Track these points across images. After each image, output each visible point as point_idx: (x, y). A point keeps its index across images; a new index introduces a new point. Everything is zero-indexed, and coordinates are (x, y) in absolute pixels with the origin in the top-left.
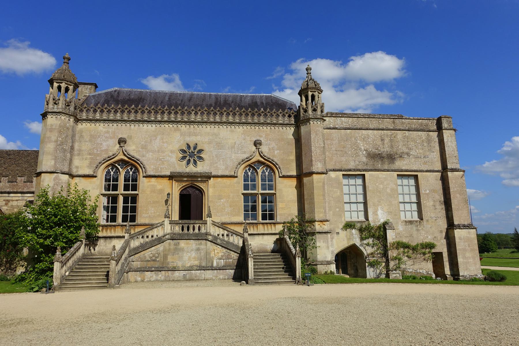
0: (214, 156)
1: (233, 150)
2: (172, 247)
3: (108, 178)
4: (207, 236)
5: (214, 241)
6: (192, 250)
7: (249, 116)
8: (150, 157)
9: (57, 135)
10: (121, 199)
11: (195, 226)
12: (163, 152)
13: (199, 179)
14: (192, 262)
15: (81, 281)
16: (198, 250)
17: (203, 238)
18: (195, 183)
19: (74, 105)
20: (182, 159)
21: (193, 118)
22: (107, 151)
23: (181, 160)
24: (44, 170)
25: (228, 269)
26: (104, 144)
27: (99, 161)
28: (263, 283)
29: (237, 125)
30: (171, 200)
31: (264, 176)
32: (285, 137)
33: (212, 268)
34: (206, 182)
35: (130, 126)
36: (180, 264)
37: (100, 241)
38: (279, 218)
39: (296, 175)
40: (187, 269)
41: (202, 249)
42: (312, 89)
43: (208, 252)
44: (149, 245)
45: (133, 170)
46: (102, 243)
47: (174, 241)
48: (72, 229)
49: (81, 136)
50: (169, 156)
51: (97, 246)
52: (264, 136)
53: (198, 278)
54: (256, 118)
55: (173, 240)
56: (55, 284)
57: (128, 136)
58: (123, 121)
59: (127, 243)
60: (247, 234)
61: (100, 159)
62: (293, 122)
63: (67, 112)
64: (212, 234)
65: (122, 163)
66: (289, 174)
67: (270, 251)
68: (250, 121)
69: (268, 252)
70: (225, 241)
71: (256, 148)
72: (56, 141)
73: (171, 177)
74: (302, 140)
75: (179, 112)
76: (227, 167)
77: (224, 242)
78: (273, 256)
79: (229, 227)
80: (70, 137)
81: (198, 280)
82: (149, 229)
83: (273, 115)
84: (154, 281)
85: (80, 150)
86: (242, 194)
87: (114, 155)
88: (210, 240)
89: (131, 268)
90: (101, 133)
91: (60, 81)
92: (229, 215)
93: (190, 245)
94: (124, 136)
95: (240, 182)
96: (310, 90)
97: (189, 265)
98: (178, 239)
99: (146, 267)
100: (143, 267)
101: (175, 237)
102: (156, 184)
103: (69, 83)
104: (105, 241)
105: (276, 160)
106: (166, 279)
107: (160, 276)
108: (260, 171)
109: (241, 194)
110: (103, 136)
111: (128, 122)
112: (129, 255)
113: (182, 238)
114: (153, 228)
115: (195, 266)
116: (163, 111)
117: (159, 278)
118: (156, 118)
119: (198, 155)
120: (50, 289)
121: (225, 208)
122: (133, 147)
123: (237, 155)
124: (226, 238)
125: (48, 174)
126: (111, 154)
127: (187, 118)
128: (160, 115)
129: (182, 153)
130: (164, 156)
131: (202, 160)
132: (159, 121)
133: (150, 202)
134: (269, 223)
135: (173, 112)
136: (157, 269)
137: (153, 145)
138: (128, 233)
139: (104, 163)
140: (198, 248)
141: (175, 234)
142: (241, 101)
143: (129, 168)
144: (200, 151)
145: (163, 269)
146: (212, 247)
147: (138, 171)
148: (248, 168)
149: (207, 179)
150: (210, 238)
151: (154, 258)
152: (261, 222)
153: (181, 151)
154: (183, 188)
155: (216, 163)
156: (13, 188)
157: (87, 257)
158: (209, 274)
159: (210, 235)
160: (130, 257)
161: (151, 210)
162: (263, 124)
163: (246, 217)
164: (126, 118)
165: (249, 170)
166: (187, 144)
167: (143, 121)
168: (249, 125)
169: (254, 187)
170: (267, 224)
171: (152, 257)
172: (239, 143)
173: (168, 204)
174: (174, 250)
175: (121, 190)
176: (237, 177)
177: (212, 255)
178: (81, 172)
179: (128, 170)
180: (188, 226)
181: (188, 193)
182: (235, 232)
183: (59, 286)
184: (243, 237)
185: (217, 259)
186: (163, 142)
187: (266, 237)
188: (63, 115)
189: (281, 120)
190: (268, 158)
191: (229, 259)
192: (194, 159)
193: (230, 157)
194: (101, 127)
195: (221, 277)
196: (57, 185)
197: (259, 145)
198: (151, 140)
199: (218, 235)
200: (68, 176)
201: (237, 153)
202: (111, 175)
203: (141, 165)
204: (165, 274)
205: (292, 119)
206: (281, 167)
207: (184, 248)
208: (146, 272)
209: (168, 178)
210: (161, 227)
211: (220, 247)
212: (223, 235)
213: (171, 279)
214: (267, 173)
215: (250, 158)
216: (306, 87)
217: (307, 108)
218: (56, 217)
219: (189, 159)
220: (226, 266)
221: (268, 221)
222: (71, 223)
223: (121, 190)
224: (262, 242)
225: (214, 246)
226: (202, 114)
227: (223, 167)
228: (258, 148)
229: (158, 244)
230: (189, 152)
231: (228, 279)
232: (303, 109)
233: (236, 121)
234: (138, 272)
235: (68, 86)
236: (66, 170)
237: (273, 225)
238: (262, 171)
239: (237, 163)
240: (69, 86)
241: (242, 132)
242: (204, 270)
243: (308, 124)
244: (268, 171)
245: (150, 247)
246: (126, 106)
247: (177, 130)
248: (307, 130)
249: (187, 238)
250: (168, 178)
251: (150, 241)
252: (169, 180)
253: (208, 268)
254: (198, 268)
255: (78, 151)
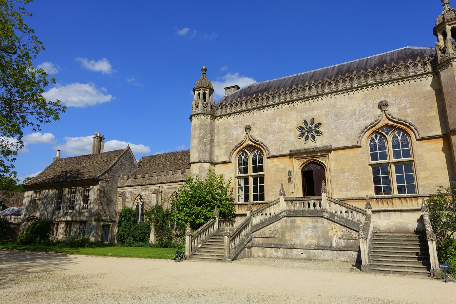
0: (333, 128)
1: (354, 118)
2: (289, 224)
3: (240, 162)
4: (323, 214)
5: (332, 218)
6: (309, 228)
7: (369, 77)
8: (272, 138)
9: (199, 132)
10: (251, 180)
11: (310, 203)
12: (282, 132)
13: (319, 154)
14: (310, 241)
15: (207, 253)
16: (315, 227)
17: (319, 215)
18: (316, 159)
19: (210, 105)
20: (300, 136)
21: (308, 94)
22: (237, 139)
23: (300, 137)
24: (192, 162)
25: (350, 251)
26: (235, 133)
27: (232, 149)
28: (381, 271)
29: (356, 89)
30: (293, 178)
31: (396, 142)
32: (420, 90)
33: (331, 249)
34: (326, 156)
35: (253, 114)
36: (297, 242)
37: (238, 218)
38: (421, 191)
39: (441, 134)
40: (304, 248)
41: (319, 227)
42: (451, 21)
43: (325, 230)
44: (267, 223)
45: (259, 153)
46: (239, 220)
47: (290, 218)
48: (209, 208)
49: (219, 130)
50: (288, 135)
51: (235, 223)
52: (390, 95)
53: (316, 258)
54: (378, 77)
55: (289, 217)
56: (187, 254)
57: (252, 123)
58: (247, 110)
59: (249, 221)
60: (370, 211)
61: (232, 147)
62: (430, 70)
63: (205, 112)
64: (329, 210)
65: (250, 148)
66: (430, 134)
67: (413, 231)
68: (371, 82)
69: (410, 233)
70: (344, 219)
71: (382, 111)
72: (199, 137)
73: (291, 155)
74: (444, 88)
75: (294, 91)
76: (349, 138)
77: (343, 220)
78: (407, 238)
79: (347, 203)
80: (209, 132)
81: (317, 260)
82: (267, 206)
83: (400, 69)
84: (274, 258)
85: (218, 142)
86: (370, 165)
87: (243, 142)
88: (326, 217)
89: (254, 244)
90: (232, 125)
91: (206, 89)
92: (355, 190)
93: (306, 223)
94: (249, 124)
95: (366, 151)
96: (447, 24)
97: (306, 244)
98: (293, 217)
99: (266, 244)
100: (264, 244)
101: (291, 214)
102: (278, 163)
103: (205, 89)
104: (241, 218)
105: (409, 120)
106: (285, 257)
107: (279, 253)
108: (390, 138)
109: (368, 166)
110: (234, 127)
111: (251, 111)
112: (252, 231)
113: (298, 216)
114: (270, 206)
115: (313, 245)
116: (279, 94)
117: (279, 255)
118: (274, 101)
119: (316, 129)
120: (182, 258)
121: (350, 182)
122: (257, 132)
123: (359, 123)
124: (345, 215)
125: (195, 164)
126: (240, 141)
127: (302, 95)
128: (277, 98)
129: (300, 130)
130: (283, 136)
131: (320, 134)
132: (276, 104)
133: (275, 181)
134: (413, 197)
135: (288, 92)
136: (276, 246)
137: (274, 127)
138: (249, 211)
139: (235, 150)
140: (315, 225)
141: (290, 211)
142: (367, 64)
143: (255, 152)
144: (318, 125)
145: (281, 247)
146: (330, 225)
147: (263, 154)
148: (374, 135)
149: (327, 153)
150: (326, 215)
151: (273, 235)
152: (397, 196)
153: (299, 128)
154: (304, 165)
155: (336, 135)
156: (184, 178)
157: (220, 232)
158: (328, 255)
159: (327, 212)
160: (252, 233)
161: (276, 188)
162: (387, 81)
163: (378, 191)
164: (249, 108)
165: (376, 137)
166: (304, 121)
167: (263, 107)
168: (370, 87)
169: (384, 156)
170: (405, 198)
171: (271, 234)
172: (360, 109)
173: (291, 182)
174: (291, 228)
175: (251, 172)
176: (360, 147)
177: (330, 233)
178: (220, 160)
179: (255, 153)
180: (309, 202)
181: (309, 170)
182: (354, 209)
183: (190, 256)
184: (365, 214)
185: (336, 238)
186: (282, 123)
187: (405, 214)
188: (202, 115)
189: (412, 72)
190: (398, 120)
191: (350, 239)
192: (312, 135)
193: (351, 126)
194: (231, 120)
195: (343, 259)
196: (202, 172)
197: (384, 107)
198: (271, 123)
199: (336, 212)
200: (209, 164)
201: (359, 121)
202: (242, 160)
203: (264, 147)
204: (284, 251)
205: (429, 66)
206: (418, 127)
207: (300, 225)
208: (267, 249)
209: (289, 157)
210: (277, 205)
211: (339, 225)
212: (341, 212)
213: (290, 257)
214: (400, 138)
215: (375, 123)
216: (442, 21)
217: (446, 47)
218: (195, 198)
219: (308, 136)
220: (347, 247)
221: (259, 202)
222: (207, 203)
223: (251, 172)
224: (400, 220)
225: (332, 224)
226: (317, 87)
227: (344, 138)
228: (384, 111)
229: (275, 222)
230: (307, 128)
231: (350, 262)
232: (440, 50)
233: (355, 85)
234: (260, 248)
235: (205, 92)
236: (207, 159)
237: (414, 200)
238: (393, 136)
239: (360, 131)
240: (206, 91)
241: (362, 96)
242: (323, 250)
243: (450, 66)
244: (401, 135)
245: (268, 224)
246: (249, 97)
247: (294, 108)
248: (449, 74)
249: (302, 215)
250: (289, 157)
251: (269, 218)
252: (290, 158)
253: (327, 248)
254: (316, 248)
255: (217, 142)
